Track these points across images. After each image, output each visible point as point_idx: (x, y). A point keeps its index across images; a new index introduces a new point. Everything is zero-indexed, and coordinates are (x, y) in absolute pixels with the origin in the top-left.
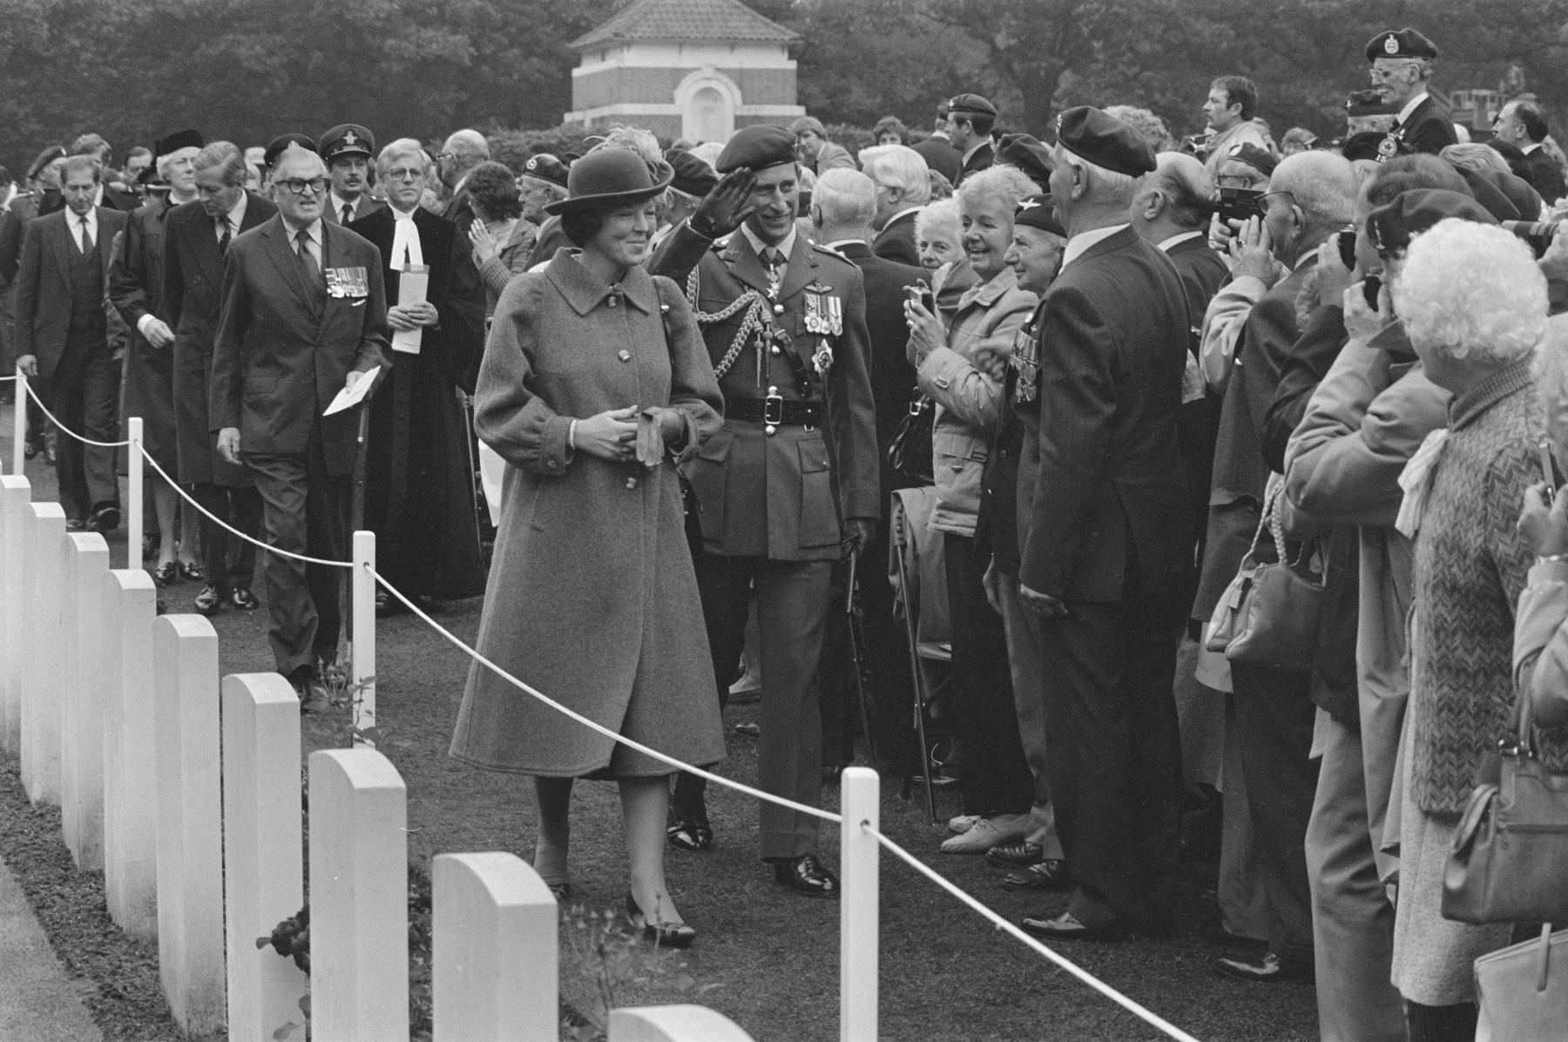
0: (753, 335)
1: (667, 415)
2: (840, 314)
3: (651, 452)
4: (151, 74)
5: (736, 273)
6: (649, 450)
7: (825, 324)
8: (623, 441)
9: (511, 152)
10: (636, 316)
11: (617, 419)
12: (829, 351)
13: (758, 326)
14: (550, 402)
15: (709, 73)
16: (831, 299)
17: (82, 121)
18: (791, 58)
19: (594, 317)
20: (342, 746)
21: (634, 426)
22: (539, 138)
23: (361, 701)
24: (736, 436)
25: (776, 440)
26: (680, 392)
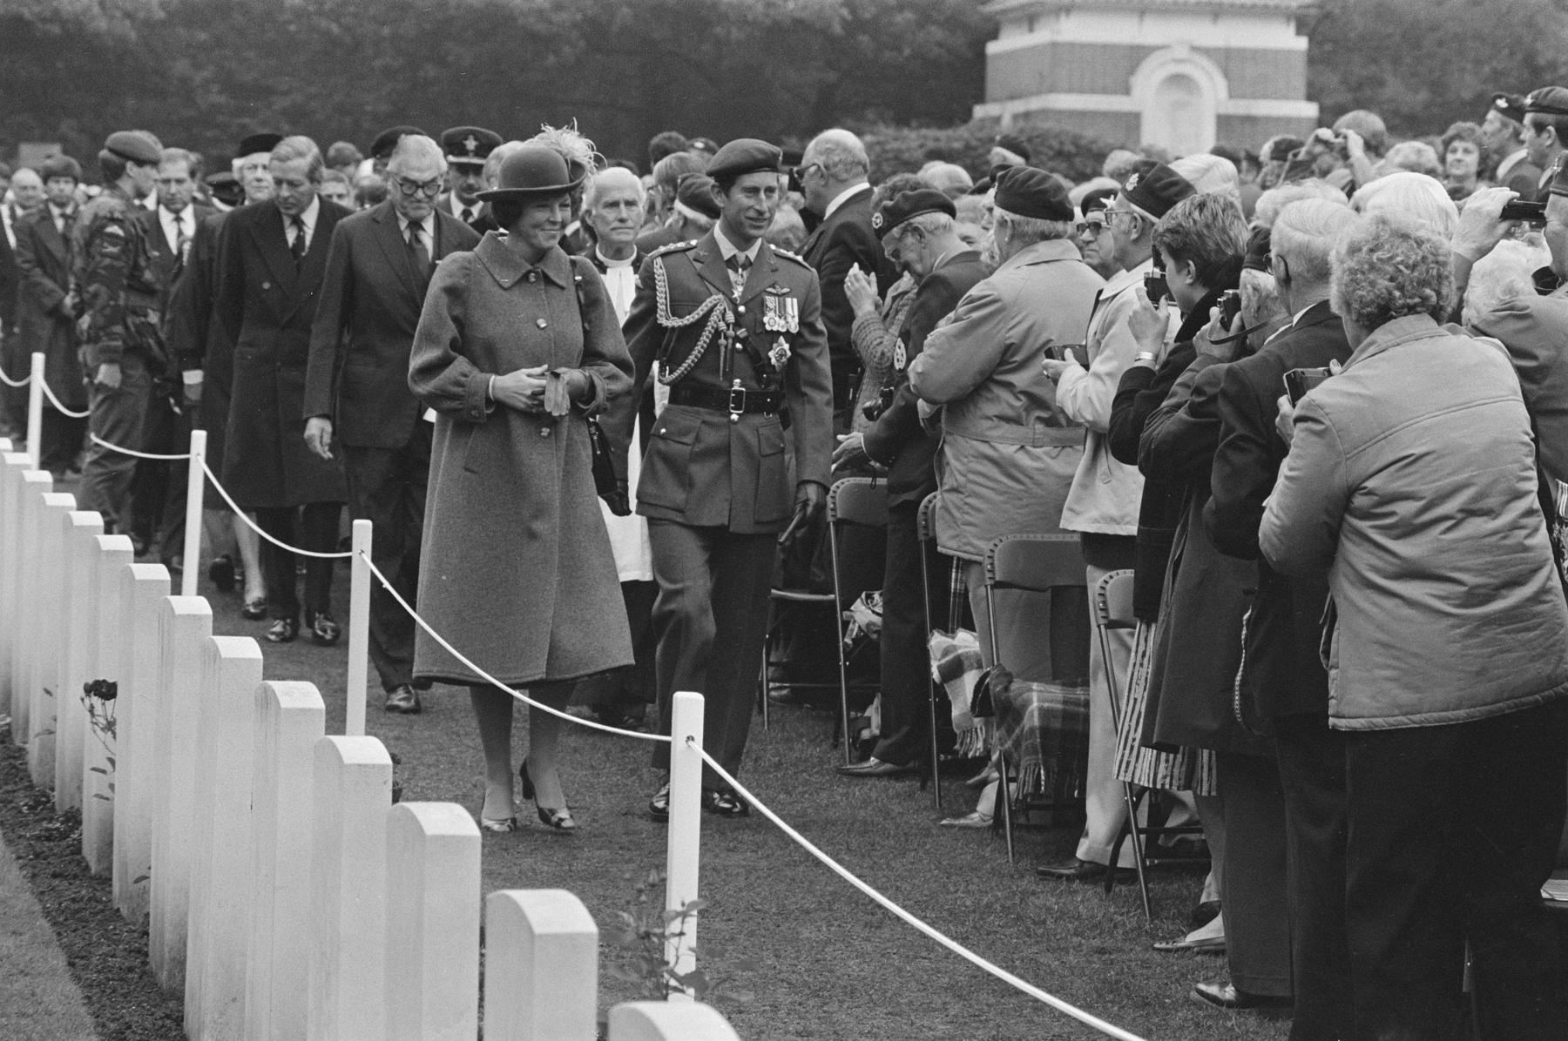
0: (717, 334)
1: (575, 375)
2: (796, 313)
3: (557, 405)
4: (386, 31)
5: (703, 273)
6: (557, 402)
7: (782, 322)
8: (534, 395)
9: (896, 158)
10: (554, 291)
11: (529, 376)
12: (786, 346)
13: (722, 326)
14: (474, 362)
15: (1183, 53)
16: (788, 300)
17: (285, 94)
18: (1299, 32)
19: (516, 291)
20: (652, 998)
21: (543, 382)
22: (937, 140)
23: (681, 934)
24: (704, 422)
25: (740, 427)
26: (591, 356)
